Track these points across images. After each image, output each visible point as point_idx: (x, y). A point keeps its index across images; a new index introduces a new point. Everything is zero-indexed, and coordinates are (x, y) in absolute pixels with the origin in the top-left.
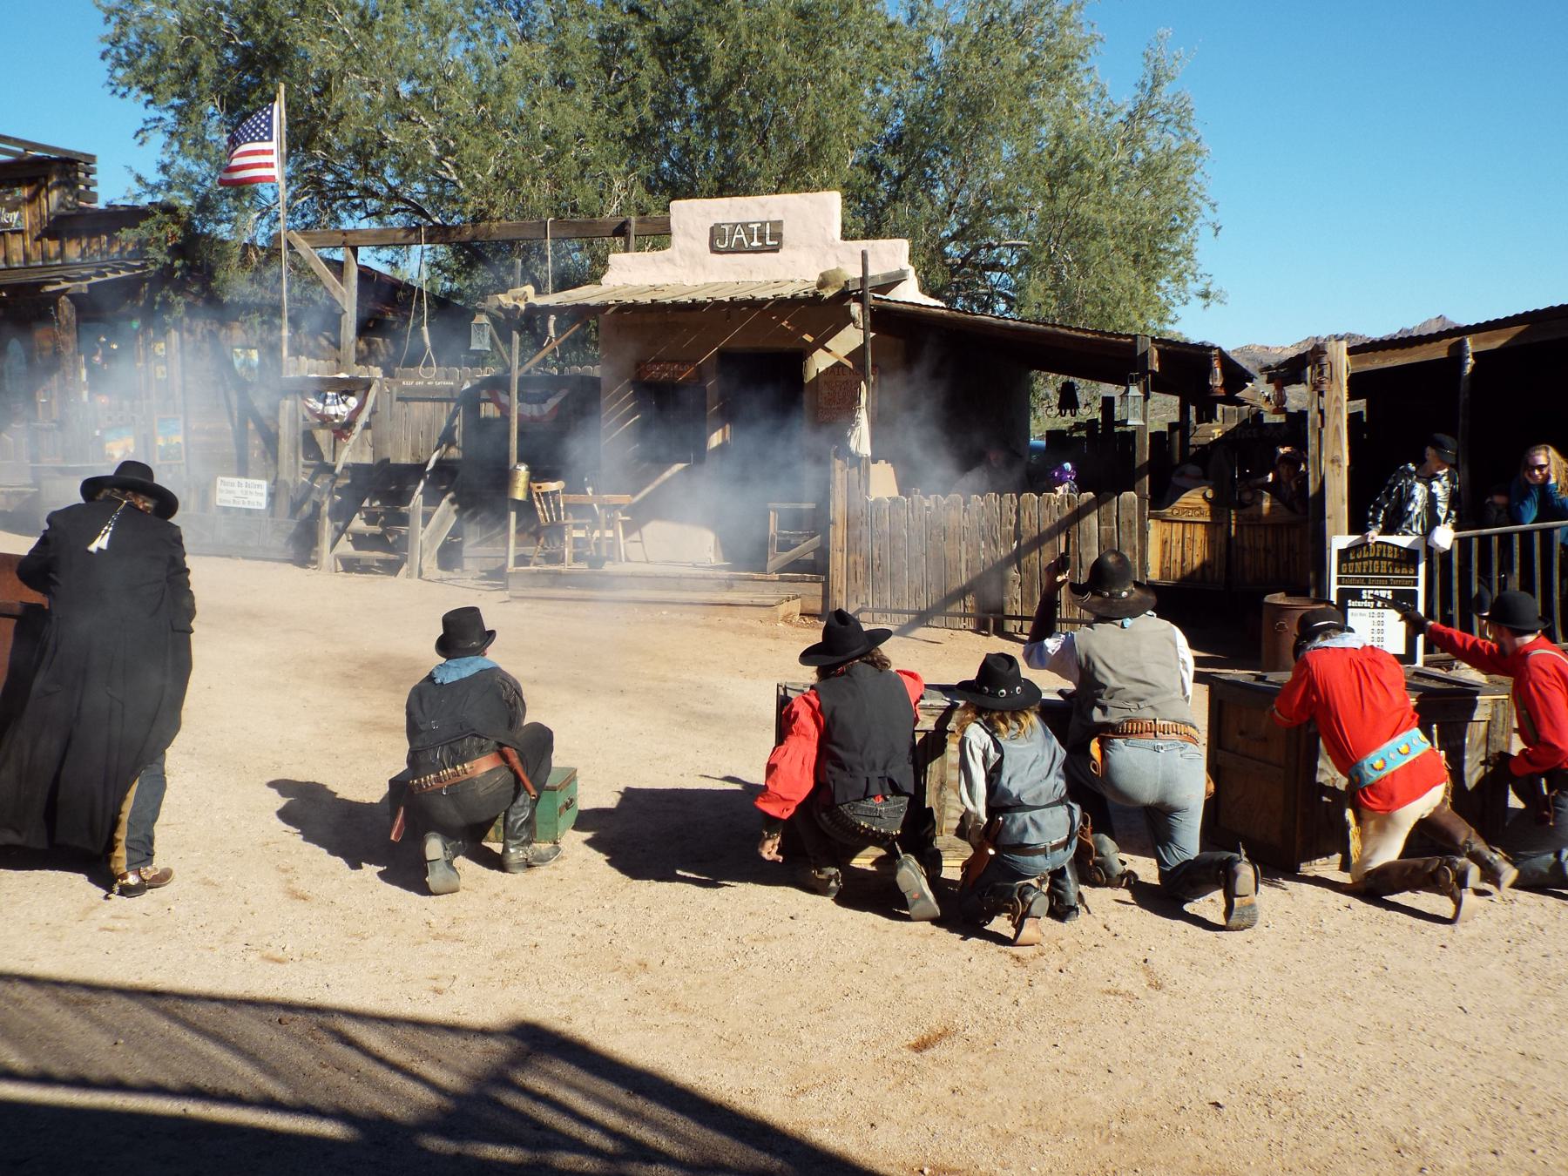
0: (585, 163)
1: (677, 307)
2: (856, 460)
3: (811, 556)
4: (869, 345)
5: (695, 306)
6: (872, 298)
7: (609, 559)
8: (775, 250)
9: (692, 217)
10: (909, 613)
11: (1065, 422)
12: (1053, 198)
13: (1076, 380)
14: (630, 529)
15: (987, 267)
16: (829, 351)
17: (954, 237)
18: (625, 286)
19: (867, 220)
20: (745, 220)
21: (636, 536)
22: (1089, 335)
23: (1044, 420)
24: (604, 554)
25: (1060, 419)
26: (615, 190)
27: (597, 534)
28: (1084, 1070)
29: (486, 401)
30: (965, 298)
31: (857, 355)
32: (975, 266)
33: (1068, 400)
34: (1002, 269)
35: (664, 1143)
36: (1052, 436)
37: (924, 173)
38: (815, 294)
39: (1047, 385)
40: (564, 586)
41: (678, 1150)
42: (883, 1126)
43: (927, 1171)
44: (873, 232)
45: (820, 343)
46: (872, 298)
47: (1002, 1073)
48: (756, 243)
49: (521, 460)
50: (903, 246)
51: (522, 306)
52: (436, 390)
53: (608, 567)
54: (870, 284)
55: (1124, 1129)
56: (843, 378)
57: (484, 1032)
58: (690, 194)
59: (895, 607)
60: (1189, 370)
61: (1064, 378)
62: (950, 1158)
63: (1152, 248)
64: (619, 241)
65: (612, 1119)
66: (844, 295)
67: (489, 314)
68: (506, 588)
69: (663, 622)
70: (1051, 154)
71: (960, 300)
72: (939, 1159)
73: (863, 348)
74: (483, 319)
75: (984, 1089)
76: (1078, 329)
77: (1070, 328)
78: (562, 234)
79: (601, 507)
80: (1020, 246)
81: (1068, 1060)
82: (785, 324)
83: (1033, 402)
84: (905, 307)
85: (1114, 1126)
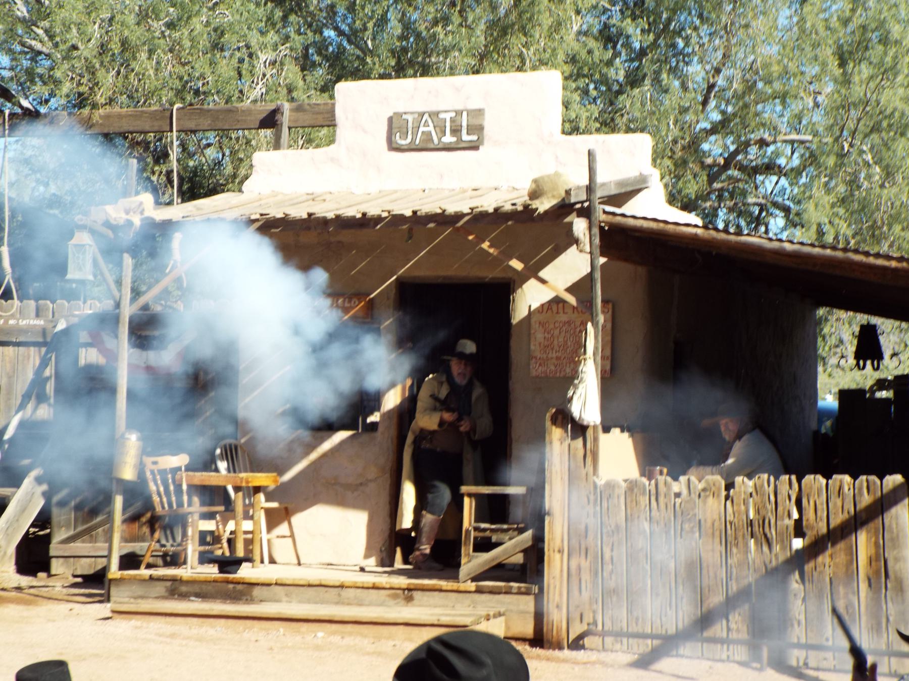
0: (220, 32)
1: (342, 223)
2: (579, 429)
3: (519, 559)
4: (598, 275)
5: (365, 222)
6: (601, 212)
7: (248, 559)
8: (474, 147)
9: (365, 103)
10: (652, 637)
11: (866, 378)
12: (846, 81)
13: (875, 320)
14: (274, 519)
15: (756, 170)
16: (543, 281)
17: (713, 130)
18: (275, 194)
19: (601, 102)
20: (434, 108)
21: (283, 529)
22: (894, 264)
23: (835, 377)
24: (240, 553)
25: (857, 374)
26: (260, 68)
27: (231, 526)
30: (731, 210)
31: (581, 288)
32: (742, 168)
33: (868, 348)
34: (780, 171)
36: (845, 396)
37: (674, 46)
38: (526, 207)
39: (840, 328)
40: (184, 596)
44: (608, 125)
45: (533, 271)
46: (601, 212)
48: (448, 139)
49: (130, 426)
50: (644, 143)
51: (137, 221)
53: (245, 572)
54: (599, 193)
56: (563, 318)
58: (360, 74)
59: (634, 629)
61: (863, 318)
64: (267, 134)
66: (564, 208)
67: (92, 232)
68: (107, 599)
69: (317, 648)
70: (846, 22)
71: (722, 213)
73: (590, 277)
74: (83, 238)
76: (877, 255)
77: (867, 254)
78: (192, 125)
79: (237, 489)
80: (802, 142)
82: (485, 245)
83: (822, 351)
84: (645, 224)
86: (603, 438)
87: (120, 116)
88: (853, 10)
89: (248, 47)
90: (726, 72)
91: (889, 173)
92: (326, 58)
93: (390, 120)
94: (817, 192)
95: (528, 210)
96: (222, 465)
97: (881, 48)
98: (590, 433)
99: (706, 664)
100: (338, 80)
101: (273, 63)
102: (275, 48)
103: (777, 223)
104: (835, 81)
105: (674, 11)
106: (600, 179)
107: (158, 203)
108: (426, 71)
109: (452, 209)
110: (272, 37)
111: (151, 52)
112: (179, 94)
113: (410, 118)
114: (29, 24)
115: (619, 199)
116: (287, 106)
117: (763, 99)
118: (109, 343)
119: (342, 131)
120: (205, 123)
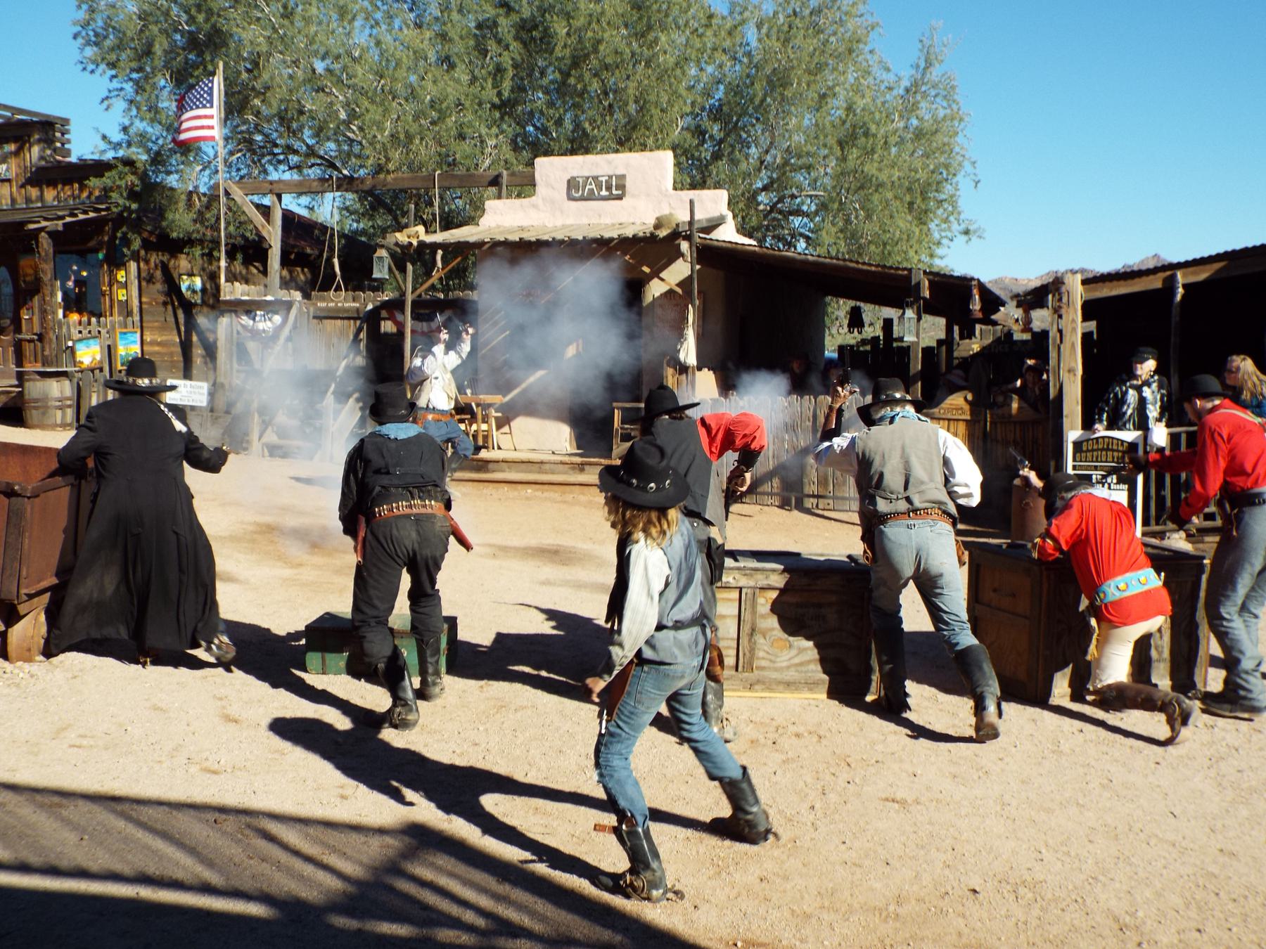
4: (695, 276)
6: (698, 237)
8: (620, 198)
9: (553, 171)
11: (852, 339)
13: (862, 305)
16: (662, 280)
18: (498, 227)
19: (694, 174)
20: (595, 174)
21: (506, 429)
23: (836, 337)
24: (480, 443)
25: (849, 336)
27: (474, 427)
28: (867, 863)
29: (385, 319)
30: (773, 237)
31: (685, 284)
32: (780, 212)
33: (856, 320)
35: (526, 921)
36: (841, 349)
38: (652, 234)
39: (839, 309)
41: (537, 927)
42: (704, 908)
43: (739, 944)
45: (656, 274)
46: (698, 237)
47: (801, 866)
48: (604, 193)
50: (723, 195)
51: (415, 243)
52: (347, 310)
55: (900, 911)
57: (381, 831)
58: (548, 153)
60: (954, 297)
61: (851, 303)
62: (758, 933)
63: (923, 198)
64: (493, 190)
65: (484, 902)
66: (676, 235)
67: (388, 249)
70: (844, 122)
72: (750, 935)
73: (690, 278)
75: (786, 878)
77: (857, 262)
78: (446, 184)
79: (478, 405)
81: (854, 855)
85: (891, 908)
86: (698, 373)
87: (403, 179)
88: (847, 115)
89: (480, 136)
90: (773, 152)
91: (869, 217)
92: (529, 144)
93: (569, 181)
94: (828, 225)
95: (653, 237)
96: (469, 391)
97: (863, 139)
98: (690, 371)
99: (759, 507)
100: (536, 156)
101: (495, 147)
102: (497, 136)
103: (801, 245)
104: (837, 159)
105: (740, 116)
106: (697, 217)
107: (427, 232)
108: (587, 151)
109: (607, 235)
110: (495, 130)
111: (422, 139)
112: (439, 165)
113: (604, 179)
114: (347, 123)
115: (709, 229)
116: (505, 172)
117: (796, 169)
118: (399, 317)
119: (541, 188)
120: (456, 183)
